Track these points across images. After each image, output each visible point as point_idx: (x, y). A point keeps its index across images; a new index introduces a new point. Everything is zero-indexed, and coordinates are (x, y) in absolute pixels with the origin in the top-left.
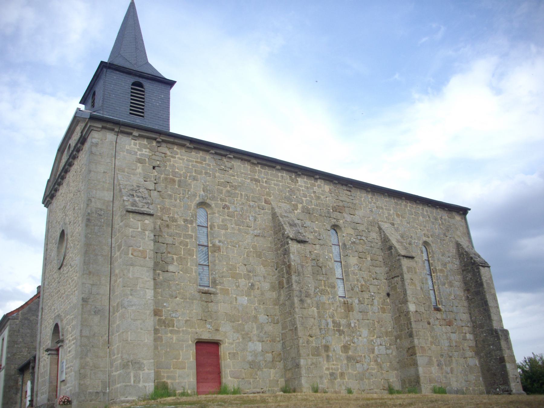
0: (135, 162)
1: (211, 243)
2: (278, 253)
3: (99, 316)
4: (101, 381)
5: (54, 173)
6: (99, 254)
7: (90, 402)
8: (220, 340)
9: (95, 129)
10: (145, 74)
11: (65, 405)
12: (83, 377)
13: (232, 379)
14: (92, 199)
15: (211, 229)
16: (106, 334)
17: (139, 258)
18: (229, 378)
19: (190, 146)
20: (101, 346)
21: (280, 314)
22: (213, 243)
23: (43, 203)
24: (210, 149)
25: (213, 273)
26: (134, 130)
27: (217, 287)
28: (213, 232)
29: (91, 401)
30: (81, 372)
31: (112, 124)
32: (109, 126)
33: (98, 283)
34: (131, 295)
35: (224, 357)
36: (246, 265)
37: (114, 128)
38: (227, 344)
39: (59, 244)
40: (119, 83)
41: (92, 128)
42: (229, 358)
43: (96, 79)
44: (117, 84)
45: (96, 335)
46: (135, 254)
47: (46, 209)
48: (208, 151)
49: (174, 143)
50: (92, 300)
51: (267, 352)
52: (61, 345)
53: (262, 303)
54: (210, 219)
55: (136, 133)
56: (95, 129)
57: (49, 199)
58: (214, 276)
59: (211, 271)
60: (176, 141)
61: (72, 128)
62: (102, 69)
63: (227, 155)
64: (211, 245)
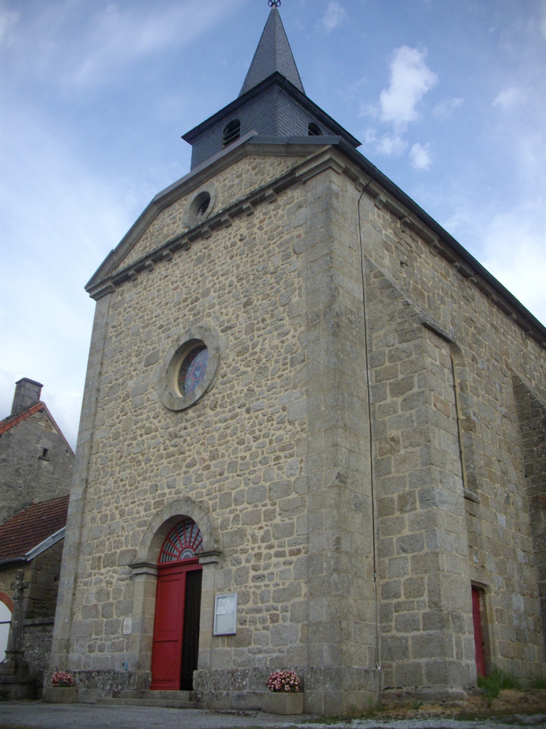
0: (381, 246)
1: (464, 415)
2: (533, 450)
3: (361, 514)
4: (369, 647)
5: (130, 241)
6: (355, 394)
7: (358, 692)
8: (485, 585)
9: (335, 167)
10: (325, 116)
11: (293, 691)
12: (346, 637)
13: (502, 657)
14: (339, 288)
15: (462, 389)
16: (370, 552)
17: (443, 415)
18: (499, 656)
19: (438, 245)
20: (366, 577)
21: (535, 551)
22: (467, 415)
23: (86, 288)
24: (455, 259)
25: (469, 466)
26: (383, 191)
27: (478, 490)
28: (465, 396)
29: (359, 690)
30: (342, 626)
31: (359, 169)
32: (354, 170)
33: (357, 449)
34: (441, 482)
35: (491, 616)
36: (499, 461)
37: (359, 176)
38: (493, 594)
39: (170, 365)
40: (295, 116)
41: (331, 164)
42: (497, 620)
43: (248, 100)
44: (292, 118)
45: (359, 552)
46: (438, 405)
47: (93, 302)
48: (450, 261)
49: (419, 233)
50: (351, 480)
51: (529, 615)
52: (216, 560)
53: (518, 530)
54: (459, 374)
55: (383, 197)
56: (335, 167)
57: (112, 285)
58: (471, 470)
59: (466, 461)
60: (426, 230)
61: (219, 166)
62: (272, 85)
63: (471, 276)
64: (464, 418)
